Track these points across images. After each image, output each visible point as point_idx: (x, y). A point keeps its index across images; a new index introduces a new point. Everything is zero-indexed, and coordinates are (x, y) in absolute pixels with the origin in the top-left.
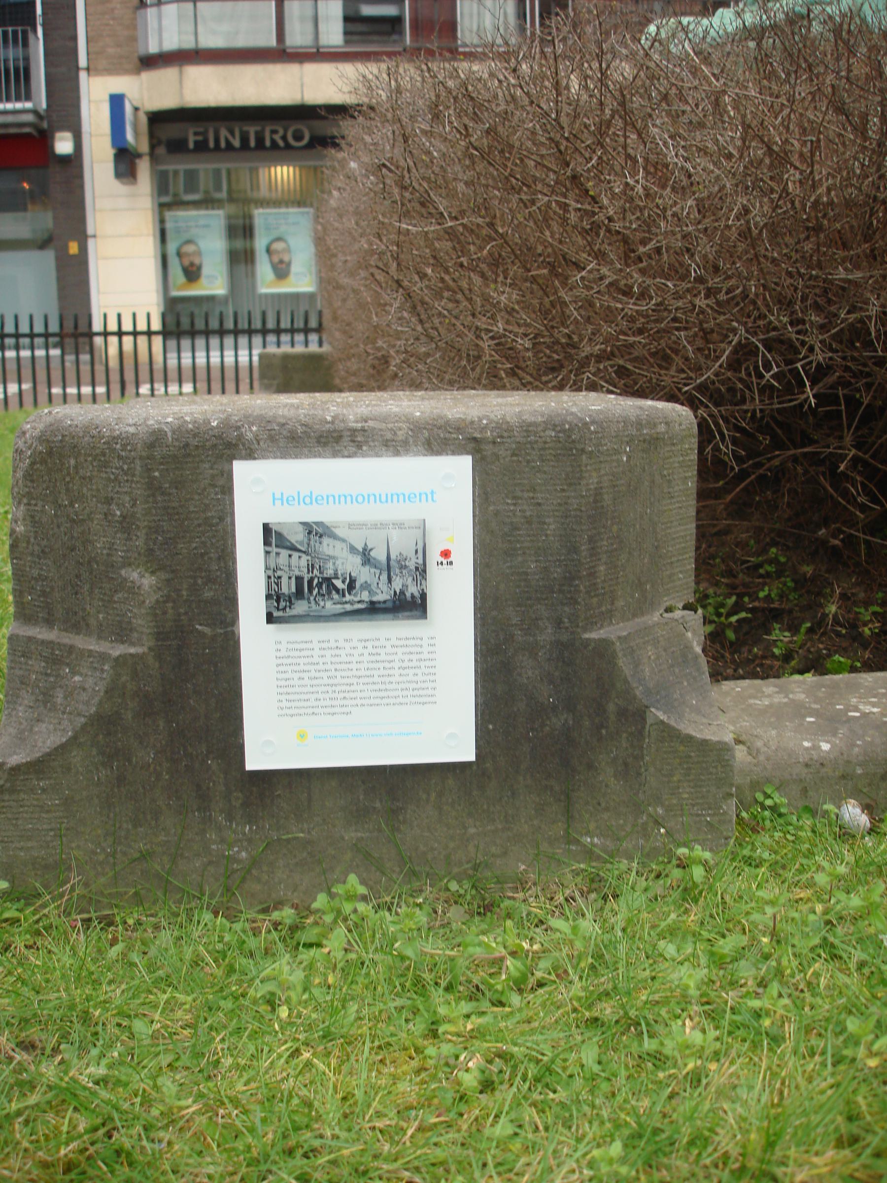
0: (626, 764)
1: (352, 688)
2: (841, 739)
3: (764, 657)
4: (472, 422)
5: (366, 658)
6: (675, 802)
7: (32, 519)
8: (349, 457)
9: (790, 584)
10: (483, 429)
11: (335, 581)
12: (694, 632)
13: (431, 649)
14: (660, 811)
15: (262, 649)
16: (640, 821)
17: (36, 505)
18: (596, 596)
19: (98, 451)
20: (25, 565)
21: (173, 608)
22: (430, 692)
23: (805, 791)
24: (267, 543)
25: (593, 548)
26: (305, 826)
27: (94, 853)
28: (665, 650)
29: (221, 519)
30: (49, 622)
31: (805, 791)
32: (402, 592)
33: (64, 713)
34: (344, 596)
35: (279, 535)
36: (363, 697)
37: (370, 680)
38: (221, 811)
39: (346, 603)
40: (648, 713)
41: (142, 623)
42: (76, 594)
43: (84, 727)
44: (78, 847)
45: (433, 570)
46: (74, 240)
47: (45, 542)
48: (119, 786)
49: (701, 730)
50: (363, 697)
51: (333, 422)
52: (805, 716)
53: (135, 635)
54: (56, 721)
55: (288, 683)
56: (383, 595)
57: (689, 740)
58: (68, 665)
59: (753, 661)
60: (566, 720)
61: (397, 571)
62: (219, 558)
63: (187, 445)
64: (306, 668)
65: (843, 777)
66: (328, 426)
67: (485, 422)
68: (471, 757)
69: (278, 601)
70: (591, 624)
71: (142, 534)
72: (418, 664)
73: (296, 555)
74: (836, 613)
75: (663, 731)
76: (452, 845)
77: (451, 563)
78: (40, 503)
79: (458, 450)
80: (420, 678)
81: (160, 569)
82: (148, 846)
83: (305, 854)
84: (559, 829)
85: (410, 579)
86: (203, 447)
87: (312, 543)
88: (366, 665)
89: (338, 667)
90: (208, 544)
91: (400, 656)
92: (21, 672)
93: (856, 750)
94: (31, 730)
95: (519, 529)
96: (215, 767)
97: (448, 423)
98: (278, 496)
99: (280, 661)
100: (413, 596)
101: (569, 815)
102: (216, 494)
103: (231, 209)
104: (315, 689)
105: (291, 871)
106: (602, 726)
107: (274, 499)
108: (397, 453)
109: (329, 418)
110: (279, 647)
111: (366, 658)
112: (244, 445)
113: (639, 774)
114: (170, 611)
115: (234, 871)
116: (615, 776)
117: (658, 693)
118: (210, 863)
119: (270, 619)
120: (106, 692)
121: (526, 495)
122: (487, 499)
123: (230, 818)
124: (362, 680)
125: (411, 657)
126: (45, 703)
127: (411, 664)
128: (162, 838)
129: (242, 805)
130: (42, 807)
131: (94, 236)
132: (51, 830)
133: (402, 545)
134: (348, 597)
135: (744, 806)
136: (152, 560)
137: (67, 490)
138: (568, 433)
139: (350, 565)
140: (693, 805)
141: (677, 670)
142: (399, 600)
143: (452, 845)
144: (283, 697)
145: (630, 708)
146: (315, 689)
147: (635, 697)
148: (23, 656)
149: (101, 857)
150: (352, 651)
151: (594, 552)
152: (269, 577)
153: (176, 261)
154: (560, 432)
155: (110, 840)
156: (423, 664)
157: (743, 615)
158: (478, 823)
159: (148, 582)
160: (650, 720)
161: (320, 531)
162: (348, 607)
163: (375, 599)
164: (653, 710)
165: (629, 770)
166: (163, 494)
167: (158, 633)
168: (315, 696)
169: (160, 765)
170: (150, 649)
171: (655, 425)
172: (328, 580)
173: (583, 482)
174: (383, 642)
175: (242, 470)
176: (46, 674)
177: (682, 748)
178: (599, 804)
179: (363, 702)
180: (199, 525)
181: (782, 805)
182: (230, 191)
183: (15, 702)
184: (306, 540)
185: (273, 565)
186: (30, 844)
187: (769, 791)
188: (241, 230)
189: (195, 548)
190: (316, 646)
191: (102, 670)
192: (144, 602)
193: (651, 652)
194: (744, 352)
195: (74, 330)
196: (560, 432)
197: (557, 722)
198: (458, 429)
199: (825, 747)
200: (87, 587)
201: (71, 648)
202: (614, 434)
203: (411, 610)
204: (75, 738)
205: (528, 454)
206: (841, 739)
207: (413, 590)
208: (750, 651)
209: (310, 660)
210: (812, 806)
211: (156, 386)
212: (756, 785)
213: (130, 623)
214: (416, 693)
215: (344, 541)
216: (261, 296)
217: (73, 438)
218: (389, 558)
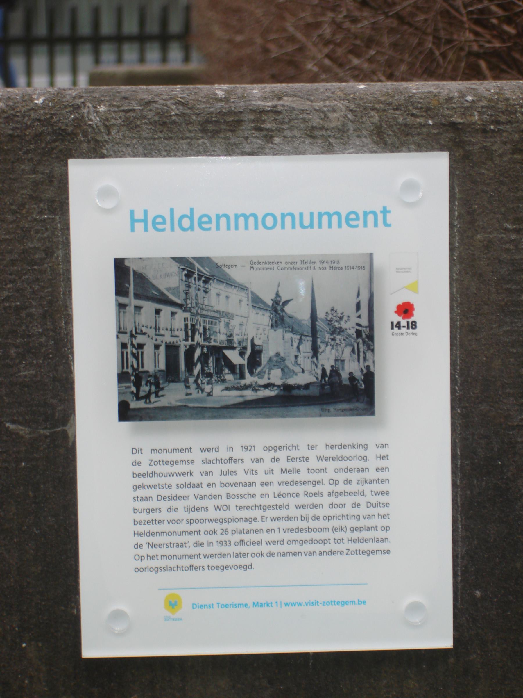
1: (254, 526)
5: (277, 476)
8: (252, 154)
13: (382, 464)
22: (380, 534)
24: (121, 290)
29: (49, 252)
32: (335, 372)
34: (242, 377)
35: (140, 278)
37: (283, 513)
39: (246, 387)
51: (226, 100)
56: (304, 376)
61: (328, 336)
62: (44, 316)
64: (181, 492)
67: (469, 98)
69: (138, 385)
72: (360, 488)
73: (166, 310)
77: (414, 325)
79: (426, 143)
80: (363, 511)
85: (348, 350)
87: (192, 291)
88: (276, 489)
98: (139, 215)
99: (139, 481)
100: (352, 378)
102: (41, 213)
104: (194, 527)
107: (133, 221)
108: (328, 149)
110: (138, 457)
111: (277, 476)
119: (125, 413)
124: (270, 513)
127: (348, 488)
133: (336, 296)
139: (252, 326)
144: (143, 540)
146: (194, 527)
152: (124, 346)
156: (367, 488)
161: (206, 271)
162: (249, 395)
163: (291, 381)
168: (195, 538)
172: (217, 351)
174: (303, 452)
175: (81, 174)
179: (273, 548)
180: (13, 262)
184: (183, 287)
189: (7, 299)
190: (198, 456)
198: (427, 110)
207: (352, 367)
209: (187, 479)
214: (356, 535)
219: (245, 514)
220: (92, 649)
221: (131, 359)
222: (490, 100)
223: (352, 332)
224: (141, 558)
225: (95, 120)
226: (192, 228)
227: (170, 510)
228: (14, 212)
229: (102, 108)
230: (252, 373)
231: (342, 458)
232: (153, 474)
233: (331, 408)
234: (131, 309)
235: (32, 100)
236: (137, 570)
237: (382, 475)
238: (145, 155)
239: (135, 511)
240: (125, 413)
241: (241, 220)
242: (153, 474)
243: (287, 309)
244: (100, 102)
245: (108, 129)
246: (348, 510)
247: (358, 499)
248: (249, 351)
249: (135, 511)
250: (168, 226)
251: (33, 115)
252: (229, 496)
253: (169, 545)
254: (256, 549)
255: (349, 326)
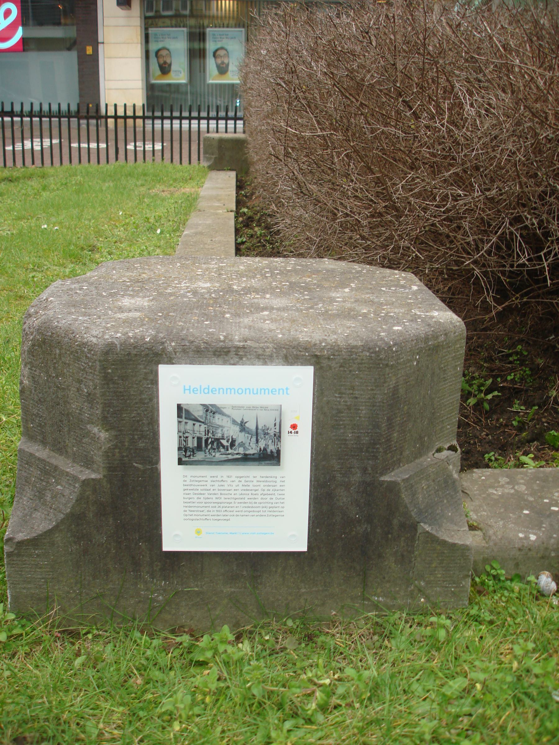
0: (403, 556)
1: (231, 505)
2: (543, 532)
3: (506, 426)
4: (315, 345)
5: (240, 487)
6: (432, 579)
7: (33, 378)
8: (234, 364)
9: (528, 372)
10: (323, 349)
11: (222, 441)
12: (454, 465)
13: (282, 484)
14: (422, 584)
15: (175, 481)
16: (409, 589)
17: (35, 371)
18: (390, 452)
19: (73, 349)
20: (28, 405)
21: (119, 452)
22: (280, 509)
23: (517, 565)
24: (179, 416)
25: (390, 424)
26: (199, 583)
27: (68, 592)
28: (434, 481)
29: (151, 400)
30: (44, 442)
31: (517, 565)
32: (265, 449)
33: (51, 508)
34: (227, 450)
35: (187, 411)
36: (237, 511)
37: (242, 501)
38: (148, 572)
39: (229, 454)
40: (419, 527)
41: (99, 458)
42: (60, 431)
43: (62, 521)
44: (59, 589)
45: (285, 436)
46: (89, 45)
47: (40, 395)
48: (84, 555)
49: (452, 536)
50: (237, 511)
51: (224, 341)
52: (523, 509)
53: (95, 466)
54: (46, 513)
55: (190, 500)
56: (253, 450)
57: (444, 543)
58: (54, 477)
59: (499, 427)
60: (366, 528)
61: (262, 436)
62: (149, 424)
63: (129, 354)
64: (202, 492)
65: (543, 557)
66: (222, 344)
67: (323, 344)
68: (305, 549)
69: (185, 451)
70: (386, 470)
71: (100, 406)
72: (273, 492)
73: (198, 424)
74: (556, 396)
75: (428, 537)
76: (290, 598)
77: (297, 432)
78: (38, 371)
79: (305, 362)
80: (274, 501)
81: (111, 429)
82: (102, 591)
83: (198, 599)
84: (358, 591)
85: (270, 441)
86: (140, 355)
87: (208, 417)
88: (240, 492)
89: (223, 492)
90: (142, 415)
91: (262, 487)
92: (25, 474)
93: (552, 541)
94: (31, 515)
95: (342, 413)
96: (144, 547)
97: (299, 344)
98: (187, 387)
99: (186, 487)
100: (272, 452)
101: (365, 584)
102: (148, 384)
103: (192, 22)
104: (207, 505)
105: (190, 608)
106: (389, 533)
107: (185, 390)
108: (265, 363)
109: (222, 338)
110: (185, 479)
111: (240, 487)
112: (166, 354)
113: (410, 562)
114: (117, 454)
115: (154, 607)
116: (395, 562)
117: (426, 512)
118: (139, 602)
119: (180, 462)
120: (77, 501)
121: (348, 392)
122: (322, 393)
123: (153, 577)
124: (237, 501)
125: (269, 488)
126: (40, 498)
127: (269, 492)
128: (110, 586)
129: (160, 569)
130: (36, 565)
131: (103, 43)
132: (43, 578)
133: (266, 420)
134: (230, 451)
135: (478, 578)
136: (106, 422)
137: (55, 368)
138: (378, 353)
139: (232, 431)
140: (444, 581)
141: (440, 493)
142: (263, 454)
143: (290, 598)
144: (187, 509)
145: (407, 522)
146: (207, 505)
147: (411, 516)
148: (27, 464)
149: (73, 595)
150: (232, 483)
151: (390, 426)
152: (180, 437)
153: (155, 60)
154: (372, 353)
155: (79, 585)
156: (276, 492)
157: (496, 393)
158: (307, 586)
159: (103, 435)
160: (419, 531)
161: (214, 410)
162: (230, 457)
163: (247, 452)
164: (422, 524)
165: (404, 559)
166: (114, 383)
167: (110, 467)
168: (207, 509)
169: (110, 544)
170: (104, 476)
171: (437, 337)
172: (218, 440)
173: (386, 385)
174: (251, 479)
175: (164, 370)
176: (41, 480)
177: (439, 547)
178: (384, 578)
179: (238, 513)
180: (136, 403)
181: (502, 575)
182: (191, 10)
183: (22, 494)
184: (204, 415)
185: (183, 430)
186: (29, 586)
187: (494, 565)
188: (198, 36)
189: (134, 417)
190: (209, 479)
191: (75, 487)
192: (101, 448)
193: (424, 484)
194: (507, 242)
195: (88, 109)
196: (372, 353)
197: (361, 529)
198: (306, 349)
199: (533, 537)
200: (66, 429)
201: (56, 468)
202: (409, 350)
203: (270, 460)
204: (56, 527)
205: (351, 366)
206: (543, 532)
207: (272, 448)
208: (498, 420)
209: (205, 487)
210: (521, 574)
211: (138, 144)
212: (486, 561)
213: (92, 458)
214: (271, 509)
215: (229, 416)
216: (208, 85)
217: (58, 336)
218: (257, 428)
219: (227, 501)
220: (166, 548)
221: (183, 442)
222: (332, 346)
223: (272, 434)
224: (186, 515)
225: (170, 349)
226: (208, 393)
227: (198, 498)
228: (137, 384)
229: (173, 344)
230: (231, 449)
231: (266, 481)
232: (191, 485)
233: (263, 463)
234: (183, 423)
235: (144, 339)
236: (185, 519)
237: (282, 488)
238: (190, 364)
239: (184, 498)
240: (180, 462)
241: (229, 390)
242: (191, 485)
243: (247, 425)
244: (173, 341)
245: (175, 353)
246: (268, 500)
247: (272, 496)
248: (230, 441)
249: (184, 498)
250: (199, 392)
251: (145, 346)
252: (221, 494)
253: (197, 511)
254: (232, 513)
255: (272, 432)
